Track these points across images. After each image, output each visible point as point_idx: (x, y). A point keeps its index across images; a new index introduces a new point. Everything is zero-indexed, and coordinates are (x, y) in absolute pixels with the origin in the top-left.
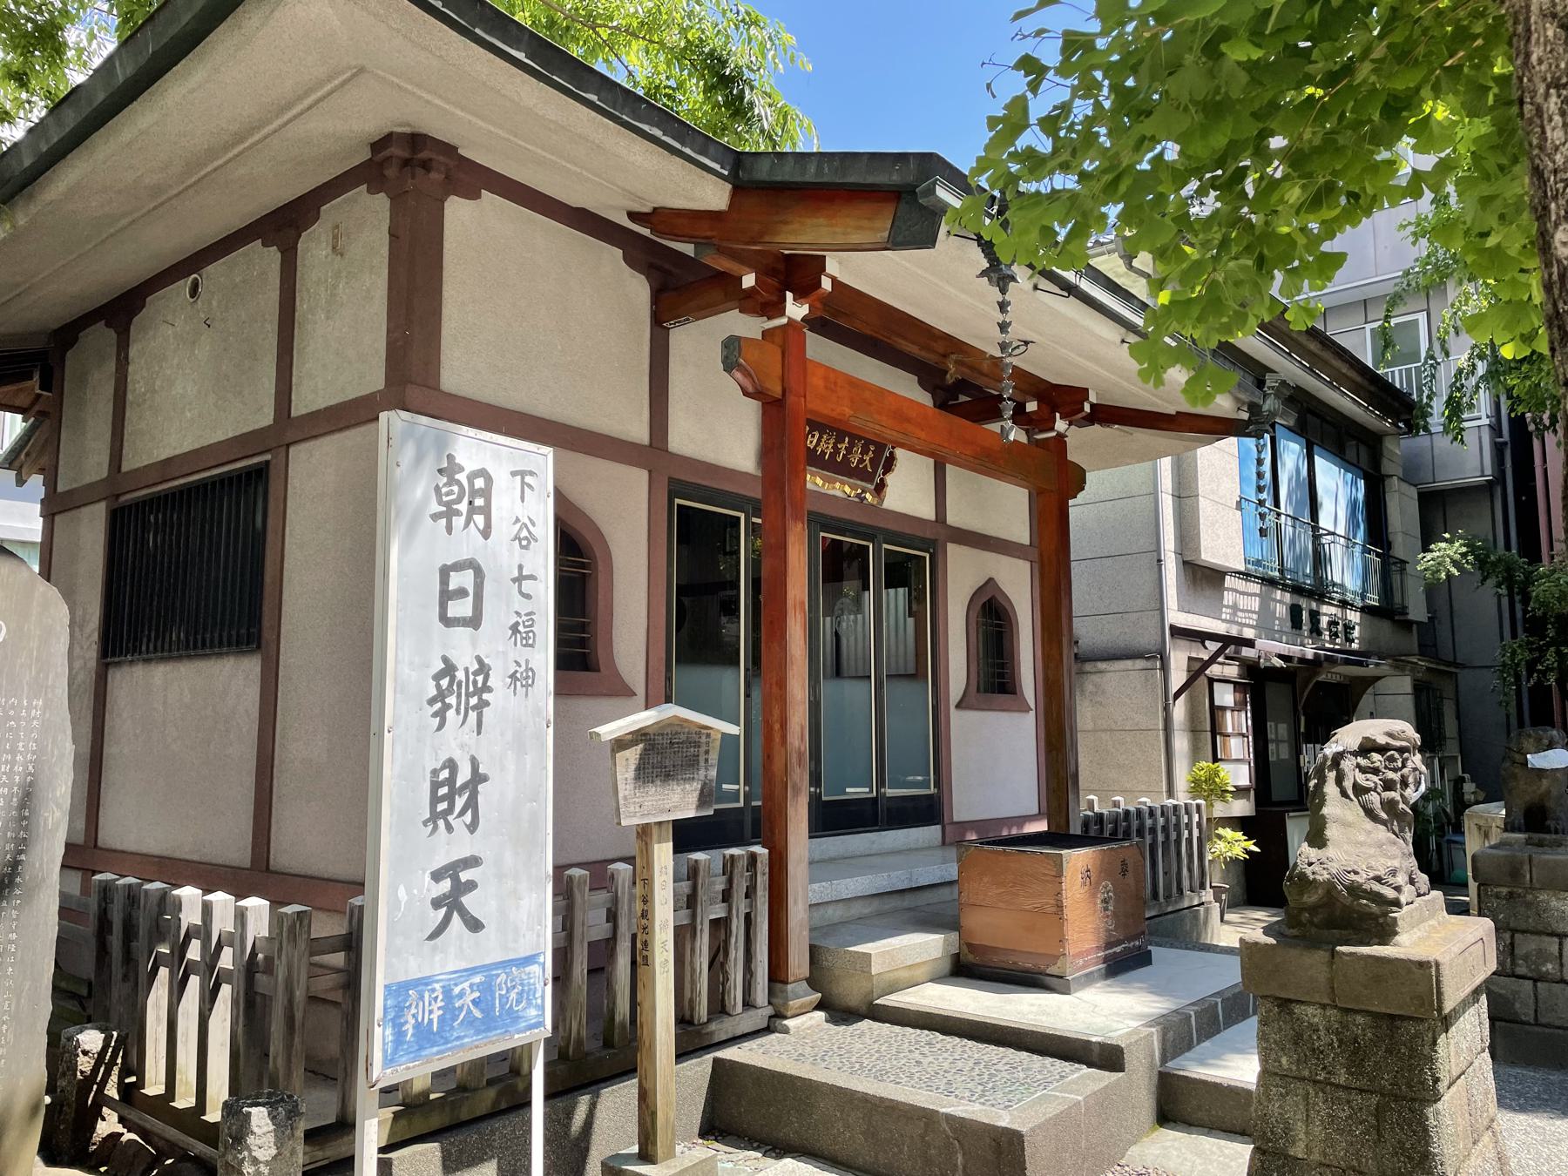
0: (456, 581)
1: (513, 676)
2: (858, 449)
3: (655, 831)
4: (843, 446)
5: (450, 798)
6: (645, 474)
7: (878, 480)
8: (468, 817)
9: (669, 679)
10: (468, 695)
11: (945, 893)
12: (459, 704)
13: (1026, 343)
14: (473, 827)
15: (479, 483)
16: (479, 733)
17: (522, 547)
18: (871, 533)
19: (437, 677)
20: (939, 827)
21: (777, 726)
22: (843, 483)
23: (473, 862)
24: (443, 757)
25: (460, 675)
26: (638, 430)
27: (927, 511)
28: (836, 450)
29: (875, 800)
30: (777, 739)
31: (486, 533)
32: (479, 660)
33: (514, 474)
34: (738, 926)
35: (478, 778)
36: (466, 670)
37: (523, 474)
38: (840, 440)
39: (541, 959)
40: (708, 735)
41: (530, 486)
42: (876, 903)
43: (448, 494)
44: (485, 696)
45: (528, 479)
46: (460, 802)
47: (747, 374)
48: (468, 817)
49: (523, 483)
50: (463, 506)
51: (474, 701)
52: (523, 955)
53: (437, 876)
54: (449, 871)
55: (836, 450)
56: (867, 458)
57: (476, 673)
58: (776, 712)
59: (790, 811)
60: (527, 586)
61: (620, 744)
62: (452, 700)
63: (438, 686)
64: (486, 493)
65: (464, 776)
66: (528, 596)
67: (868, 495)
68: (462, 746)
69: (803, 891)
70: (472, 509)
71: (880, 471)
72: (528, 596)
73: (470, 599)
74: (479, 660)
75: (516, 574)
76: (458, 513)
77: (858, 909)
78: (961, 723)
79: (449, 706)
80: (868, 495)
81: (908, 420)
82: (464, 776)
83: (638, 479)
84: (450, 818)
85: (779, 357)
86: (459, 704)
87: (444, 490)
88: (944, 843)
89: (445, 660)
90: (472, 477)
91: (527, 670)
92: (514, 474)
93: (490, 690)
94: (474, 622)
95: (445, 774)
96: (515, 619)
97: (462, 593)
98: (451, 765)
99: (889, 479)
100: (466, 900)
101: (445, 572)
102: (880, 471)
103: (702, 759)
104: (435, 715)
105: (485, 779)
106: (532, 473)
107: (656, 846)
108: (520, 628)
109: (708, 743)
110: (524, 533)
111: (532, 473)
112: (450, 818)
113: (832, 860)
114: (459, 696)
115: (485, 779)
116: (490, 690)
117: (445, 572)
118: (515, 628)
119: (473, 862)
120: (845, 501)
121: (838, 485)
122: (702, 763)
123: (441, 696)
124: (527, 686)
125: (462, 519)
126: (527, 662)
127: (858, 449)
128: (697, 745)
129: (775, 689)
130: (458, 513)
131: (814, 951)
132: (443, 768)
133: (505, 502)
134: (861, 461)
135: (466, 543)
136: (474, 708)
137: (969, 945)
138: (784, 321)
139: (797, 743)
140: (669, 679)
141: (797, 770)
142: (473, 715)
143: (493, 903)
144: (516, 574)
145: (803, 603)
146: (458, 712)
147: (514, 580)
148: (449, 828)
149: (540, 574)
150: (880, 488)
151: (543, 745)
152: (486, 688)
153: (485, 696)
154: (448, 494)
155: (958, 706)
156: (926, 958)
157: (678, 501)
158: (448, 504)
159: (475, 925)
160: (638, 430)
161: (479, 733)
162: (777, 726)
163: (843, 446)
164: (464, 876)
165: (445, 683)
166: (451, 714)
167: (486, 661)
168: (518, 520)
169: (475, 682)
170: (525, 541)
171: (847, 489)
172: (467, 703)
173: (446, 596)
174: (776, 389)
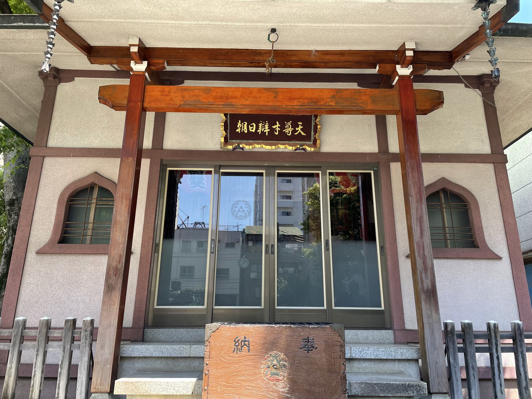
55: (272, 130)
56: (299, 129)
67: (308, 149)
134: (294, 131)
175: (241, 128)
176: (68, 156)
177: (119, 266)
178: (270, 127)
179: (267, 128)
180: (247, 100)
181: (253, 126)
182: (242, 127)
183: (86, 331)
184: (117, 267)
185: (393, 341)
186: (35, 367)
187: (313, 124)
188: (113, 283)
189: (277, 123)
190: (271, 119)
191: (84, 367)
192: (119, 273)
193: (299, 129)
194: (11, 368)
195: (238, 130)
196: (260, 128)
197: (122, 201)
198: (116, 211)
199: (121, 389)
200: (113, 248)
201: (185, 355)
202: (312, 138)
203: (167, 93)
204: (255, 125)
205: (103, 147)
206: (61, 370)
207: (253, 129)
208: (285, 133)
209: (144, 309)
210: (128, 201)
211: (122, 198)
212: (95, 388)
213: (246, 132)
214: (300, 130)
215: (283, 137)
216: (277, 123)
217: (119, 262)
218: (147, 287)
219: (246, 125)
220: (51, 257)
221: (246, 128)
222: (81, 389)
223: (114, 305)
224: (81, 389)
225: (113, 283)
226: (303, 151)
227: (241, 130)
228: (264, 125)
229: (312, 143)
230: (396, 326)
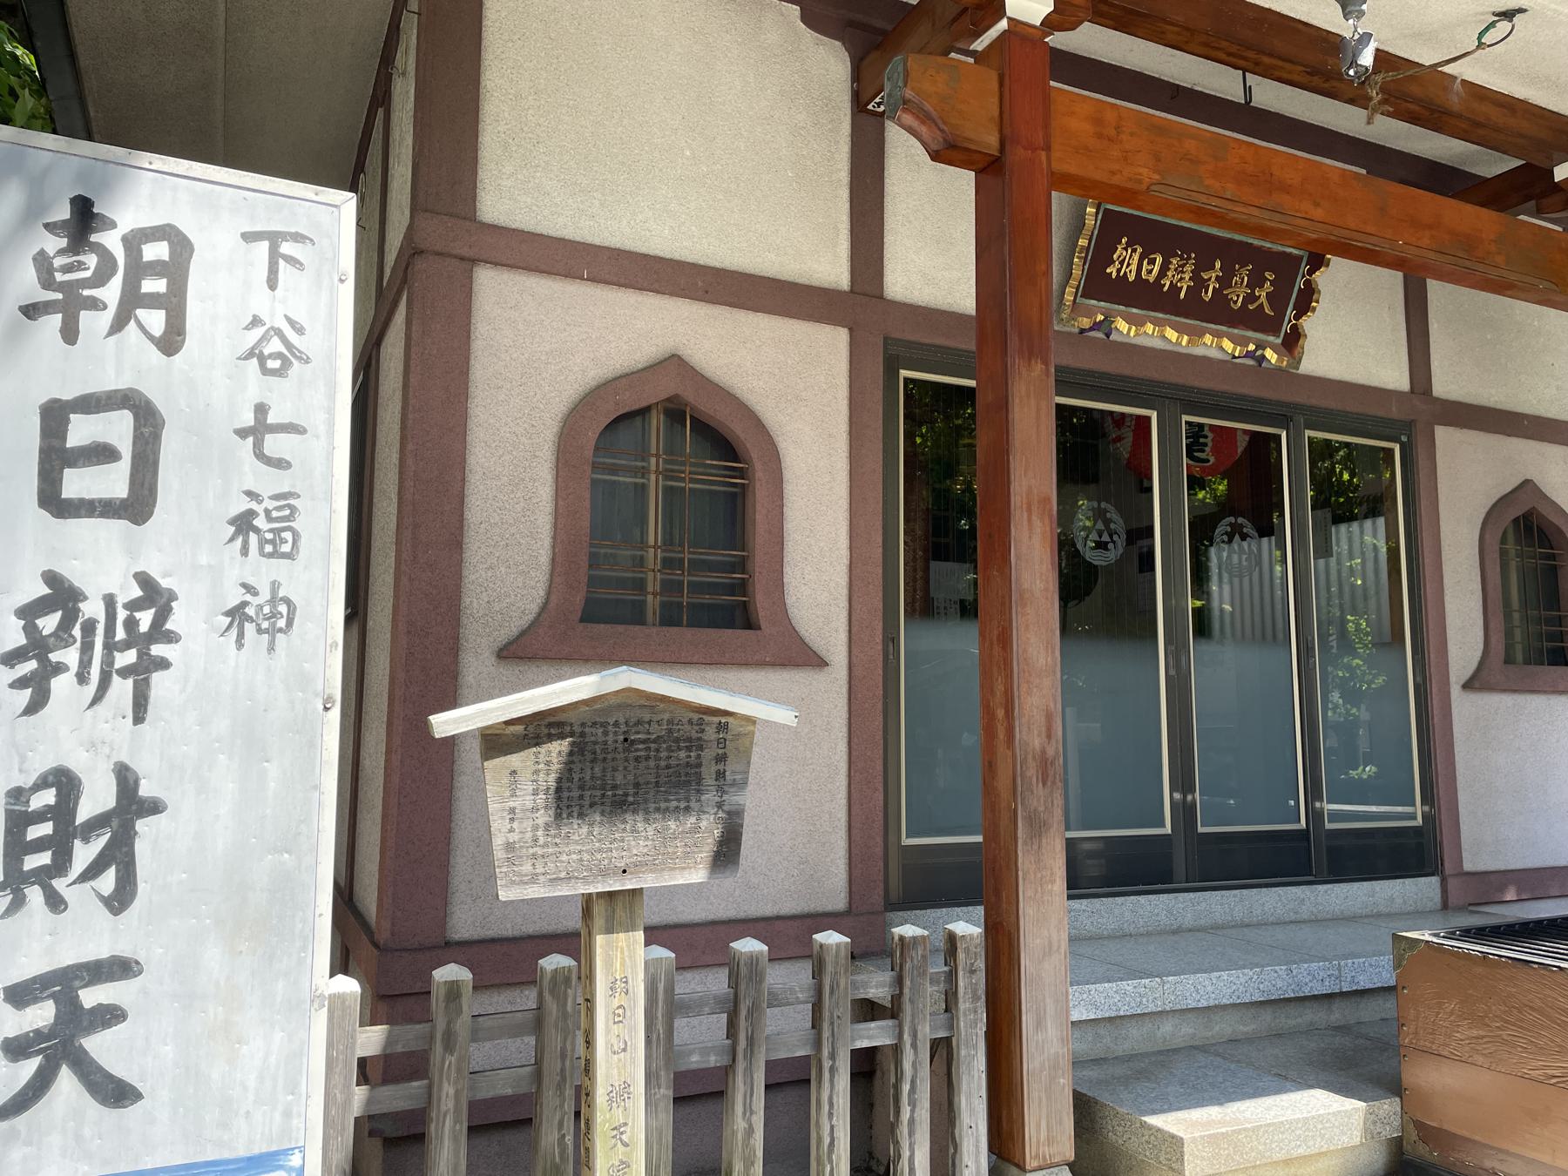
0: (81, 430)
1: (237, 614)
2: (1243, 276)
3: (598, 909)
4: (1212, 276)
5: (61, 848)
6: (841, 336)
7: (1286, 327)
8: (107, 881)
9: (891, 639)
10: (110, 647)
11: (1370, 1011)
12: (85, 664)
13: (1508, 15)
14: (119, 901)
15: (156, 251)
16: (139, 718)
17: (265, 371)
18: (1282, 417)
19: (29, 613)
20: (1434, 881)
21: (1000, 713)
22: (1218, 335)
23: (120, 968)
24: (41, 763)
25: (92, 608)
26: (830, 266)
27: (1393, 375)
28: (1199, 284)
29: (1303, 835)
30: (1001, 734)
31: (170, 342)
32: (144, 580)
33: (249, 237)
34: (915, 1072)
35: (133, 804)
36: (110, 601)
37: (274, 238)
38: (1204, 265)
39: (295, 1160)
40: (723, 727)
41: (291, 260)
42: (1267, 1016)
43: (68, 269)
44: (157, 650)
45: (286, 248)
46: (84, 854)
47: (924, 117)
48: (107, 881)
49: (274, 256)
50: (111, 292)
51: (128, 658)
52: (242, 1152)
53: (20, 995)
54: (61, 984)
55: (1199, 284)
56: (1262, 294)
57: (133, 606)
58: (999, 688)
59: (1025, 861)
60: (275, 444)
61: (496, 742)
62: (70, 656)
63: (30, 630)
64: (176, 270)
65: (96, 798)
66: (281, 464)
67: (1271, 355)
68: (92, 746)
69: (1064, 1003)
70: (132, 300)
71: (1290, 312)
72: (281, 464)
73: (124, 467)
74: (144, 580)
75: (248, 419)
76: (96, 305)
77: (1224, 1027)
78: (1469, 714)
79: (59, 668)
80: (1271, 355)
81: (1286, 189)
82: (96, 798)
83: (829, 346)
84: (59, 884)
85: (995, 85)
86: (85, 664)
87: (58, 262)
88: (1445, 906)
89: (51, 578)
90: (134, 242)
91: (274, 600)
92: (249, 237)
93: (171, 638)
94: (137, 506)
95: (48, 797)
96: (245, 504)
97: (102, 454)
98: (65, 783)
99: (1307, 323)
100: (100, 1046)
101: (55, 416)
102: (1290, 312)
103: (709, 772)
104: (20, 684)
105: (154, 807)
106: (298, 238)
107: (600, 940)
108: (260, 522)
109: (722, 743)
110: (275, 345)
111: (298, 238)
112: (59, 884)
113: (1216, 928)
114: (87, 648)
115: (154, 807)
116: (171, 638)
117: (55, 416)
118: (243, 524)
119: (120, 968)
120: (1226, 366)
121: (1208, 339)
122: (709, 780)
123: (37, 646)
124: (273, 632)
125: (107, 317)
126: (275, 586)
127: (1243, 276)
128: (697, 744)
129: (997, 649)
130: (96, 305)
131: (1085, 1110)
132: (42, 784)
133: (223, 289)
134: (1250, 298)
135: (114, 356)
136: (125, 672)
137: (1420, 1126)
138: (1003, 24)
139: (1036, 742)
140: (891, 639)
141: (1039, 790)
142: (122, 689)
143: (168, 1050)
144: (248, 419)
145: (1047, 500)
146: (82, 678)
147: (242, 433)
148: (55, 902)
149: (315, 420)
150: (1293, 341)
151: (312, 745)
152: (159, 632)
153: (157, 650)
154: (68, 269)
155: (1468, 686)
156: (1318, 1145)
157: (904, 373)
158: (69, 288)
159: (116, 1093)
160: (830, 266)
161: (139, 718)
162: (1000, 713)
163: (1212, 276)
164: (91, 997)
165: (49, 623)
166: (61, 685)
167: (164, 583)
168: (256, 321)
169: (131, 624)
170: (274, 357)
171: (1228, 345)
172: (108, 661)
173: (56, 457)
174: (990, 141)
175: (1122, 263)
176: (570, 274)
177: (1050, 752)
178: (1196, 276)
179: (1187, 277)
180: (1317, 205)
181: (1152, 262)
182: (1127, 262)
183: (972, 972)
184: (1044, 752)
185: (1439, 906)
186: (831, 1115)
187: (1300, 283)
188: (1041, 809)
189: (1218, 265)
190: (1205, 250)
191: (979, 1089)
192: (1051, 773)
193: (1262, 294)
194: (750, 1131)
195: (1112, 270)
196: (1170, 274)
197: (1030, 520)
198: (1018, 557)
199: (1203, 1158)
200: (1024, 688)
201: (1151, 1008)
202: (1286, 327)
203: (1113, 132)
204: (1159, 260)
205: (677, 255)
206: (913, 1111)
207: (1150, 272)
208: (1227, 300)
209: (879, 850)
210: (1047, 521)
211: (1029, 511)
212: (1037, 1156)
213: (1132, 278)
214: (1263, 299)
215: (1218, 313)
216: (1218, 265)
217: (1049, 737)
218: (880, 779)
219: (1136, 257)
220: (553, 671)
221: (1134, 267)
222: (977, 1162)
223: (1053, 882)
224: (977, 1162)
225: (1041, 809)
226: (1250, 362)
227: (1119, 271)
228: (1183, 266)
229: (1279, 341)
230: (1449, 867)
